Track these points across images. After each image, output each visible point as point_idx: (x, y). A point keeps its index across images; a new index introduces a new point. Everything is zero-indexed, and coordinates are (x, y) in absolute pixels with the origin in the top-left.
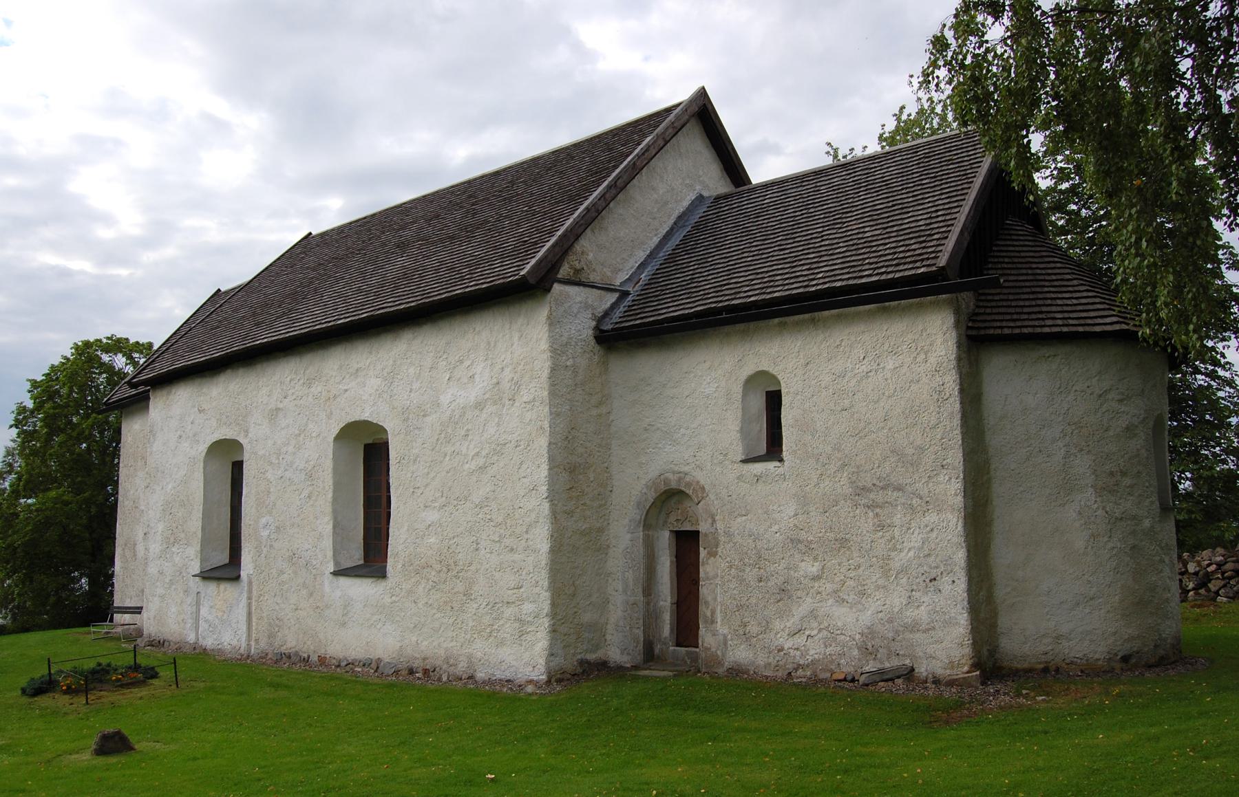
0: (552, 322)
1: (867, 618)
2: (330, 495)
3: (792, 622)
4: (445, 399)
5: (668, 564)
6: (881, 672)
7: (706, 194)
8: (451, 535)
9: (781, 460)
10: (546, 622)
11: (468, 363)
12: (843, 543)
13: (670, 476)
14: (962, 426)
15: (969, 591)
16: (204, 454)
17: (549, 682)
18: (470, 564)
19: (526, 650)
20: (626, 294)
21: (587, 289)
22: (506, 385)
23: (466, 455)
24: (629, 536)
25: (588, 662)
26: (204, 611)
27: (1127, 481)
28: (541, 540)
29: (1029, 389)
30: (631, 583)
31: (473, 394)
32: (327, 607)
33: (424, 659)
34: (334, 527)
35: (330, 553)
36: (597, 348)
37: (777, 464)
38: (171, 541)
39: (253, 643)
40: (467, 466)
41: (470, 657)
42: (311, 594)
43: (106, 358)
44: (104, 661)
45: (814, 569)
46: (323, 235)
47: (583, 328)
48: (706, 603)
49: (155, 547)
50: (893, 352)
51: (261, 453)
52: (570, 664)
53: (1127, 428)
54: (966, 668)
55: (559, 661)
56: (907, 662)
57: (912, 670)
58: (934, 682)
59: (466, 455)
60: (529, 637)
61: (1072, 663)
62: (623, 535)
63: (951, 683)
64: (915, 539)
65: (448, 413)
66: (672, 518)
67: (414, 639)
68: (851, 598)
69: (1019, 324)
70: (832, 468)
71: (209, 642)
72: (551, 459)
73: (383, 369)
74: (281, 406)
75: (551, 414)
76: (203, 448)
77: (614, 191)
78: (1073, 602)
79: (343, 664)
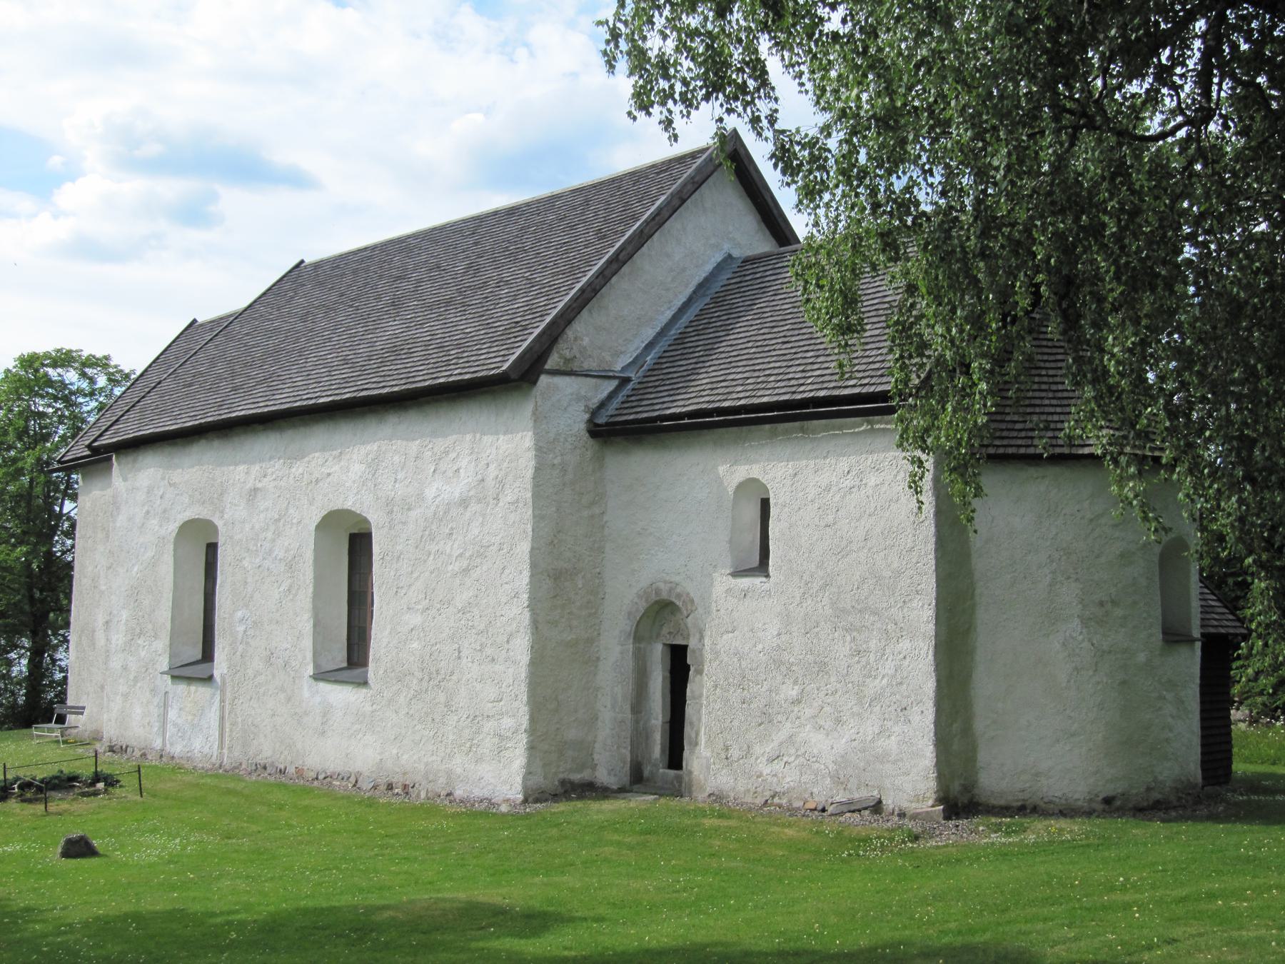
0: (537, 418)
1: (841, 744)
2: (311, 590)
3: (770, 748)
4: (430, 492)
5: (660, 679)
6: (850, 803)
7: (736, 253)
8: (433, 641)
9: (768, 576)
10: (523, 739)
11: (453, 455)
12: (822, 667)
13: (661, 585)
14: (936, 550)
15: (937, 723)
16: (174, 534)
17: (525, 801)
18: (452, 673)
19: (504, 767)
20: (625, 381)
21: (580, 379)
22: (490, 482)
23: (450, 556)
24: (618, 648)
25: (572, 783)
26: (172, 714)
27: (1118, 612)
28: (521, 649)
29: (1017, 512)
30: (620, 699)
31: (456, 490)
32: (306, 713)
33: (405, 774)
34: (315, 626)
35: (309, 655)
36: (591, 442)
37: (764, 579)
38: (135, 634)
39: (225, 751)
40: (450, 568)
41: (449, 773)
42: (289, 699)
43: (53, 373)
44: (66, 770)
45: (794, 693)
46: (317, 265)
47: (576, 421)
48: (691, 723)
49: (118, 639)
50: (876, 469)
51: (238, 537)
52: (552, 784)
53: (1122, 556)
54: (930, 802)
55: (538, 780)
56: (875, 793)
57: (880, 802)
58: (899, 815)
59: (450, 556)
60: (507, 754)
61: (1050, 802)
62: (614, 650)
63: (914, 817)
64: (888, 667)
65: (433, 508)
66: (665, 630)
67: (395, 751)
68: (828, 724)
69: (1005, 442)
70: (816, 586)
71: (177, 749)
72: (533, 566)
73: (367, 455)
74: (259, 485)
75: (534, 517)
76: (173, 527)
77: (615, 266)
78: (1052, 737)
79: (321, 777)
